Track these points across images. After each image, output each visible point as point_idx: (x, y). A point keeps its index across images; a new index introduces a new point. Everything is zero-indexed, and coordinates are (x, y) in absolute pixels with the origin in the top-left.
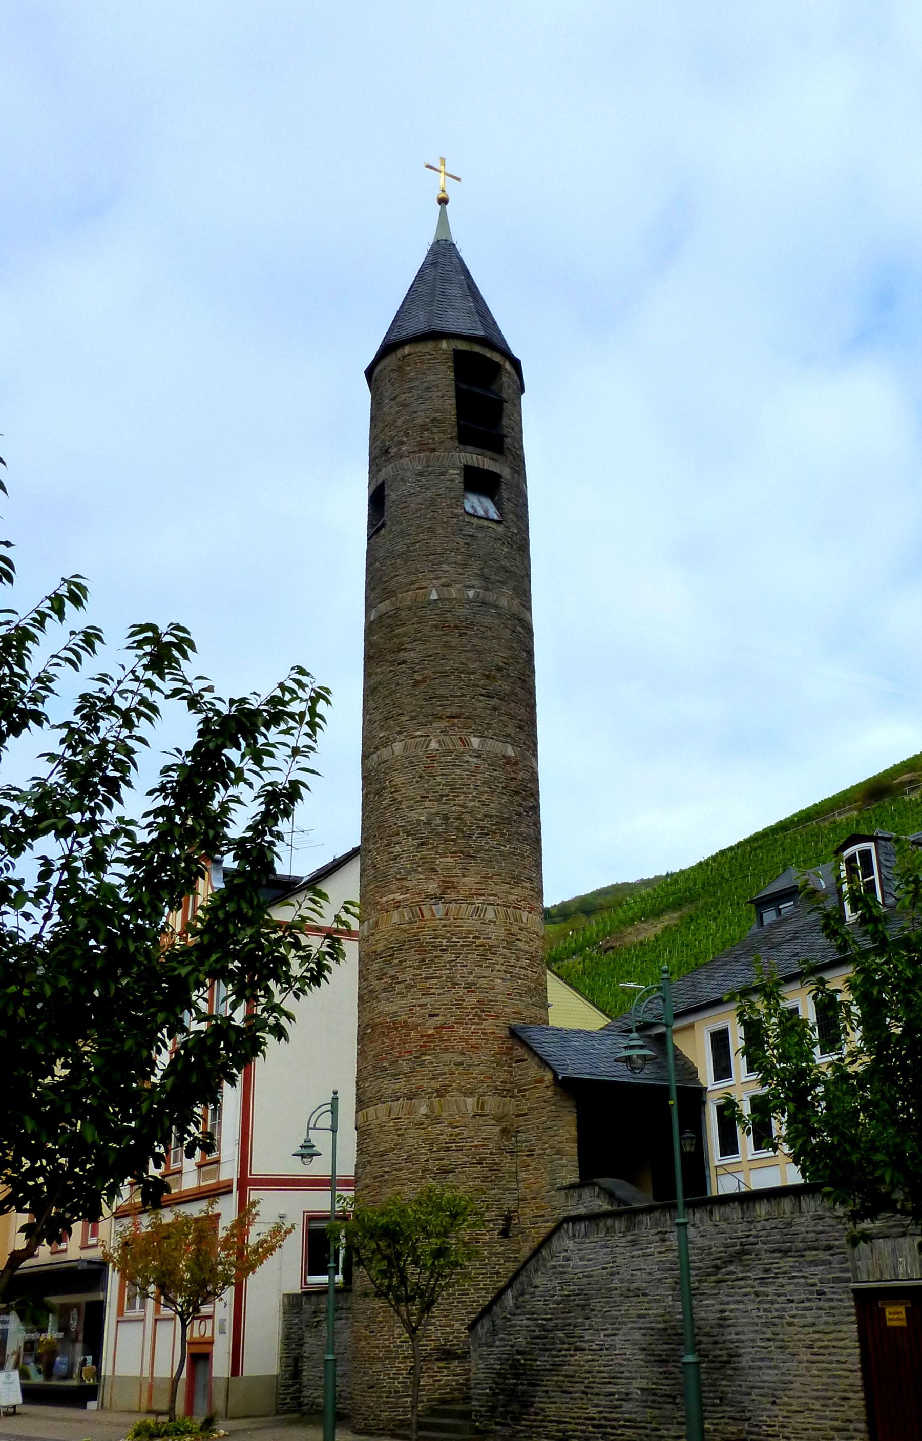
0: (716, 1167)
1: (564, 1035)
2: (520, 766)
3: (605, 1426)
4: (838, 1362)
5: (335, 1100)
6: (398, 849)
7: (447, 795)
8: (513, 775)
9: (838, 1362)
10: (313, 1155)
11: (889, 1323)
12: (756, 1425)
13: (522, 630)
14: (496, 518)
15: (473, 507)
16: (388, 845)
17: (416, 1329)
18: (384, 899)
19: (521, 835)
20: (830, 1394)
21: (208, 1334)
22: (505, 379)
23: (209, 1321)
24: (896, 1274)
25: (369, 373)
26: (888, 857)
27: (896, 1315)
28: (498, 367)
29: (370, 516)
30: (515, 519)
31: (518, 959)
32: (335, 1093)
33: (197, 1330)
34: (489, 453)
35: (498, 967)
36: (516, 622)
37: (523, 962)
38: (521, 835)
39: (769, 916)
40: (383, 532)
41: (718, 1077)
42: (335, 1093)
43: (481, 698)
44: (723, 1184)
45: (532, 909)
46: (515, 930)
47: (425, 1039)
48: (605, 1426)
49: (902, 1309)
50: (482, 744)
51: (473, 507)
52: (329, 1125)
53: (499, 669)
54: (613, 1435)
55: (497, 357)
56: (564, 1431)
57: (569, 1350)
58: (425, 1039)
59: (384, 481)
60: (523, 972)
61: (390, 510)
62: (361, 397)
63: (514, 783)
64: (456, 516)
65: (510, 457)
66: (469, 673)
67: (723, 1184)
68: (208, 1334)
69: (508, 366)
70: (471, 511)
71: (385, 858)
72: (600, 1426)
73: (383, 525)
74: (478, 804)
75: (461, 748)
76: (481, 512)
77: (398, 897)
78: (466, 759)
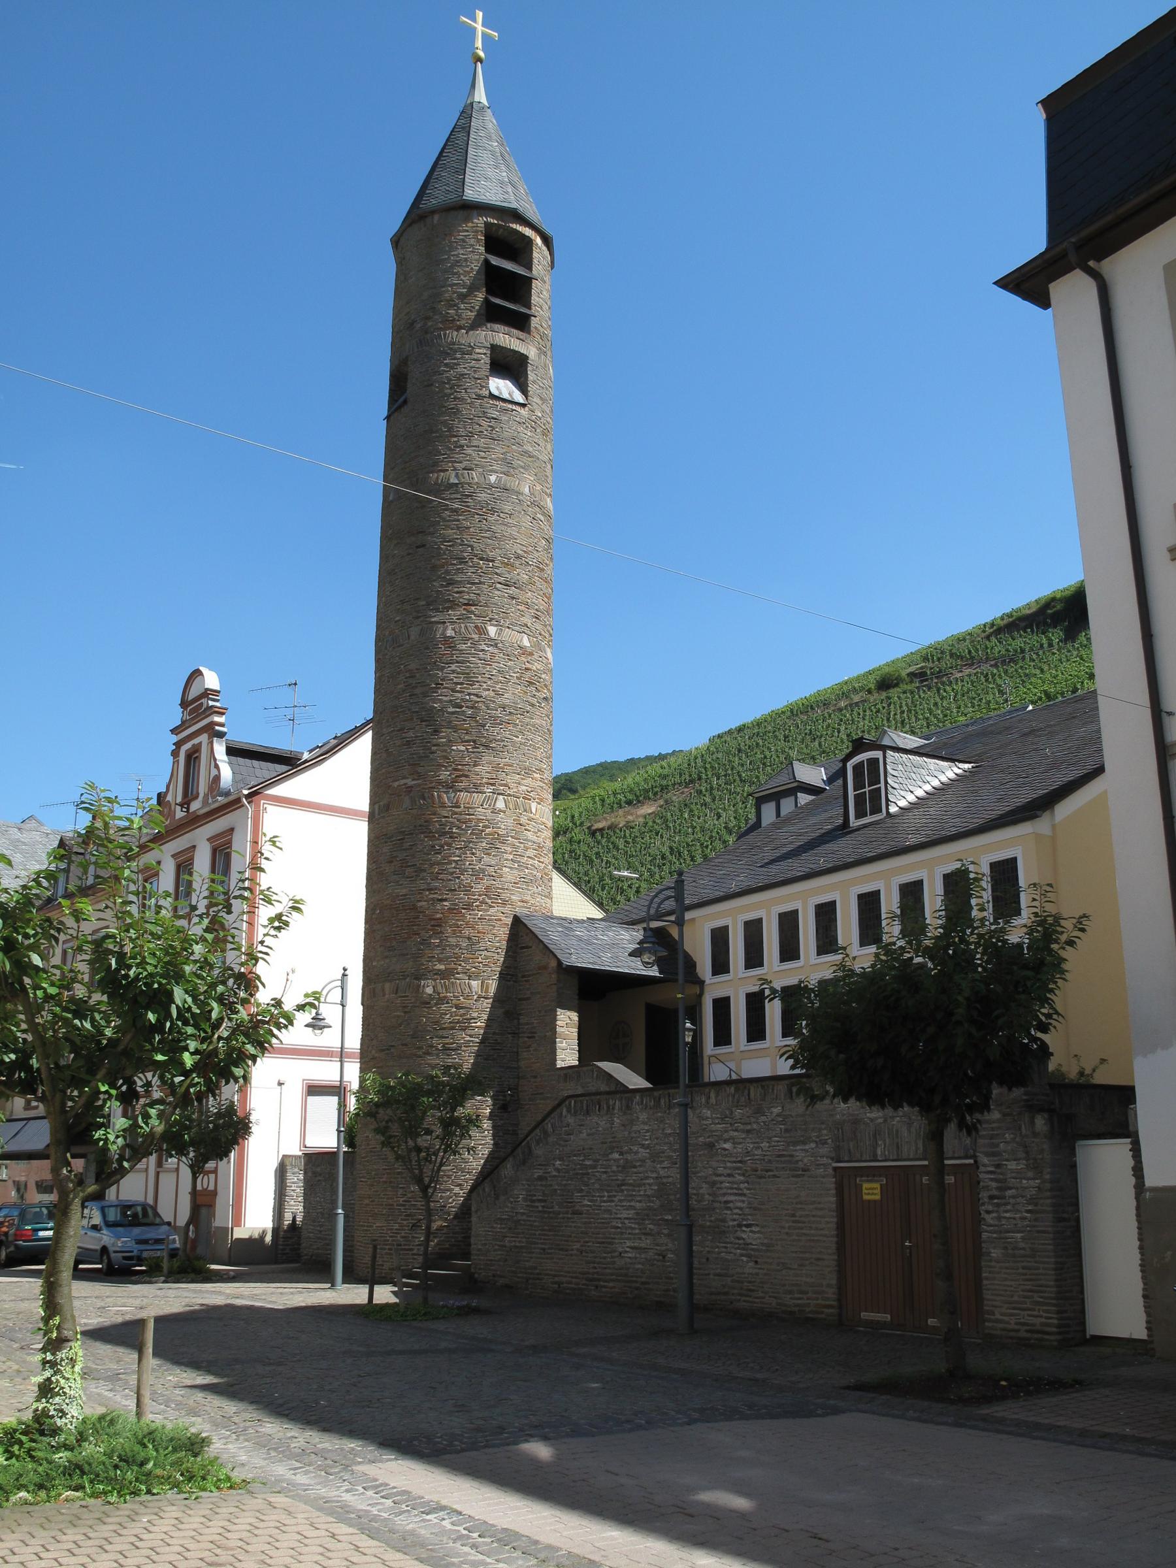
0: (710, 1057)
1: (567, 924)
2: (536, 656)
3: (599, 1280)
4: (817, 1229)
5: (344, 975)
6: (411, 734)
7: (462, 684)
8: (528, 666)
9: (817, 1229)
10: (324, 1027)
11: (866, 1197)
12: (738, 1282)
13: (542, 518)
14: (522, 401)
15: (498, 388)
16: (401, 730)
17: (428, 1186)
18: (396, 784)
19: (534, 726)
20: (807, 1255)
21: (211, 1187)
22: (535, 254)
23: (212, 1176)
24: (875, 1155)
25: (396, 242)
26: (895, 767)
27: (871, 1191)
28: (529, 242)
29: (391, 391)
30: (540, 402)
31: (526, 849)
32: (345, 970)
33: (203, 1182)
34: (515, 332)
35: (506, 856)
36: (538, 509)
37: (531, 853)
38: (534, 726)
39: (768, 813)
40: (405, 409)
41: (715, 972)
42: (345, 970)
43: (499, 586)
44: (717, 1072)
45: (541, 800)
46: (523, 820)
47: (433, 923)
48: (599, 1280)
49: (877, 1185)
50: (499, 633)
51: (498, 388)
52: (339, 1000)
53: (518, 557)
54: (605, 1287)
55: (528, 232)
56: (559, 1283)
57: (567, 1213)
58: (433, 923)
59: (407, 357)
60: (531, 862)
61: (412, 389)
62: (387, 266)
63: (528, 674)
64: (480, 397)
65: (538, 337)
66: (488, 560)
67: (717, 1072)
68: (211, 1187)
69: (539, 241)
70: (496, 393)
71: (398, 743)
72: (591, 1280)
73: (405, 402)
74: (492, 694)
75: (476, 637)
76: (506, 396)
77: (410, 782)
78: (481, 647)
